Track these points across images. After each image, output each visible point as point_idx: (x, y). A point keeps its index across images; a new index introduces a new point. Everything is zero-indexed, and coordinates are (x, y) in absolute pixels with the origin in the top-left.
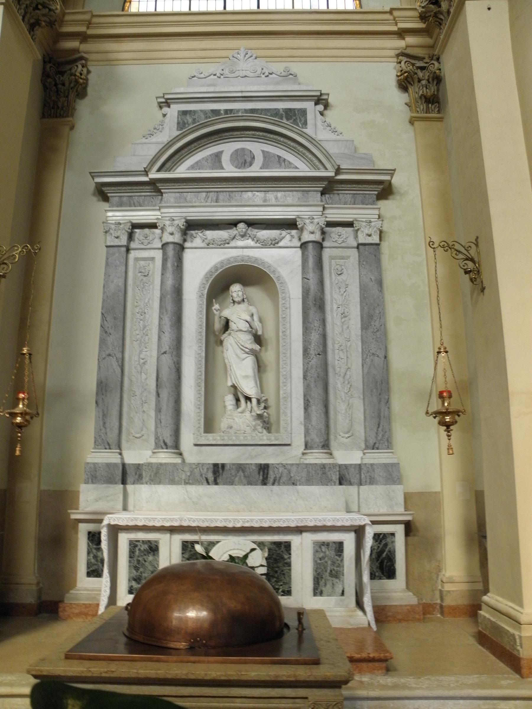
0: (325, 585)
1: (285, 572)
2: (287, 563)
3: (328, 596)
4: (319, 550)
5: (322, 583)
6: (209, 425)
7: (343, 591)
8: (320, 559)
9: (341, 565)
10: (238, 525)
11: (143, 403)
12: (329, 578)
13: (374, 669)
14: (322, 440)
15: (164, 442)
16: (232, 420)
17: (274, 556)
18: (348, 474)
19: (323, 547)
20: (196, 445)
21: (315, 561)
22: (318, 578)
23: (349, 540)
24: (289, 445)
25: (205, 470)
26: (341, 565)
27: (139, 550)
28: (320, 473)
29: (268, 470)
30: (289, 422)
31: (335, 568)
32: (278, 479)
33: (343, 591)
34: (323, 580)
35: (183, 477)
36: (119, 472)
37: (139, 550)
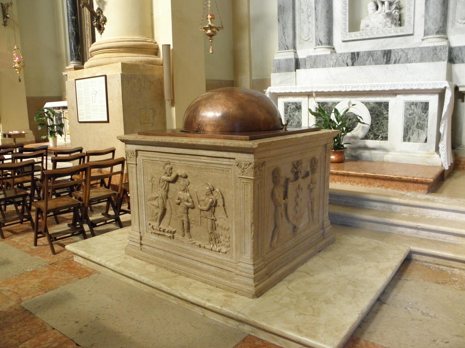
0: (413, 134)
1: (384, 123)
2: (385, 118)
3: (414, 142)
4: (409, 108)
5: (410, 132)
6: (354, 25)
7: (426, 139)
8: (410, 115)
9: (425, 120)
10: (349, 90)
11: (309, 16)
12: (415, 129)
13: (418, 189)
14: (437, 27)
15: (320, 41)
16: (368, 21)
17: (377, 112)
18: (462, 54)
19: (412, 106)
20: (344, 41)
21: (406, 116)
22: (407, 129)
23: (433, 100)
24: (412, 35)
25: (346, 57)
26: (426, 120)
27: (290, 108)
28: (432, 54)
29: (390, 55)
30: (412, 16)
31: (421, 122)
32: (397, 60)
33: (426, 139)
34: (411, 130)
35: (332, 63)
36: (293, 64)
37: (290, 108)
